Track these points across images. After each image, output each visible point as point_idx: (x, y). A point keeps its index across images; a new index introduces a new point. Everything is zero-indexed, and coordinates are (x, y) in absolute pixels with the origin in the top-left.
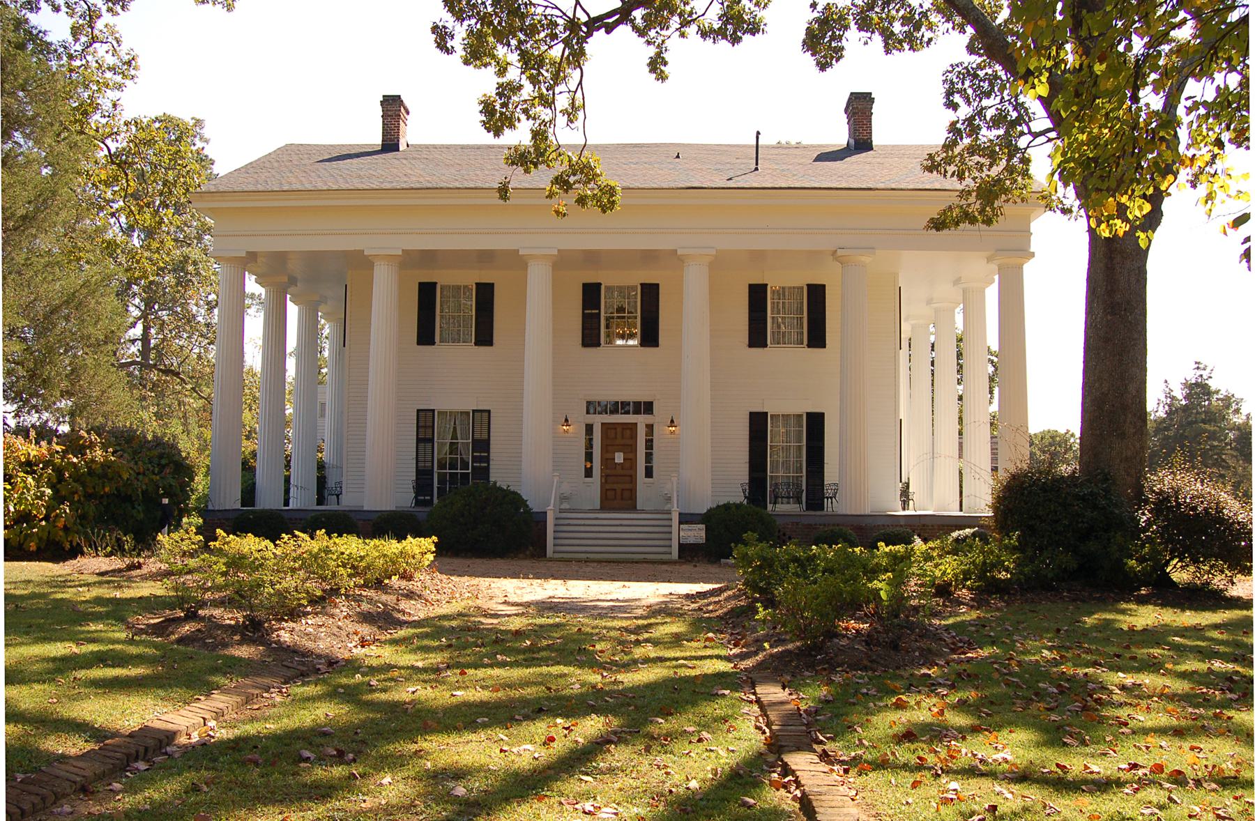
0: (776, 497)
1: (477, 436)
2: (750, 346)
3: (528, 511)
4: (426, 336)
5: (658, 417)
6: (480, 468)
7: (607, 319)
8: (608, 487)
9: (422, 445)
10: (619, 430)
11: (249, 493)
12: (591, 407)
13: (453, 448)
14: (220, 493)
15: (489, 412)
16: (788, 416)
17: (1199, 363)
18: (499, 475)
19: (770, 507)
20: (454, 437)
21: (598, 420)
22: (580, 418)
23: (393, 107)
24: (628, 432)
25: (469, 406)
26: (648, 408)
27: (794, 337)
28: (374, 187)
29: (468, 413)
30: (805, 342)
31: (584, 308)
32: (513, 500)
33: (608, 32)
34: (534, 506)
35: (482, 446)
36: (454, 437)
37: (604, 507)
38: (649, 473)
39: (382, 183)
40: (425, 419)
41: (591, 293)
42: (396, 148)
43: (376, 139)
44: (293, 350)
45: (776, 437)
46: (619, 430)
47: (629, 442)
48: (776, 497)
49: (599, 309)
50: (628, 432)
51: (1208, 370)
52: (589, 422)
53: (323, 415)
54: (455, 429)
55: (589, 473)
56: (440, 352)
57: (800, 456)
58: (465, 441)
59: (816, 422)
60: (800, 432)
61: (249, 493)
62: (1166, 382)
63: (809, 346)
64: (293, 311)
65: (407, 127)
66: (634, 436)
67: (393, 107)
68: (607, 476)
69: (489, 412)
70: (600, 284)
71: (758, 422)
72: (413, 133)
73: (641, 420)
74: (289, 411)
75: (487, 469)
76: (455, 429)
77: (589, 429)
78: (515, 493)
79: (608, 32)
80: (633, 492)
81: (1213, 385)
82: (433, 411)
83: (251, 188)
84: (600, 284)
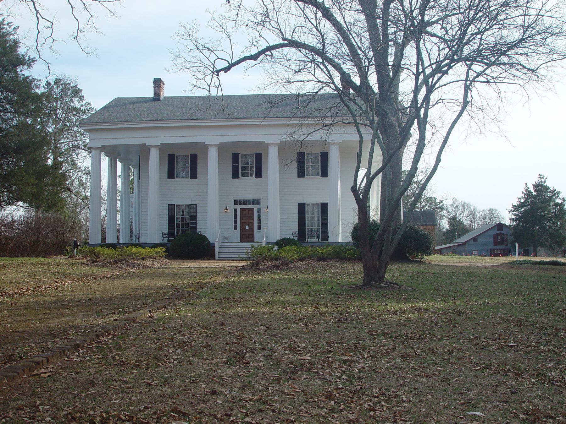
0: (309, 237)
1: (192, 214)
2: (298, 177)
3: (209, 242)
4: (171, 175)
5: (262, 206)
6: (193, 227)
7: (242, 167)
8: (243, 233)
9: (195, 214)
10: (247, 211)
11: (104, 238)
12: (236, 202)
13: (183, 219)
14: (357, 44)
15: (196, 205)
16: (314, 204)
17: (541, 175)
18: (200, 229)
19: (307, 240)
20: (183, 214)
21: (239, 207)
22: (232, 206)
23: (158, 83)
24: (251, 212)
25: (188, 202)
26: (258, 202)
27: (316, 173)
28: (149, 119)
29: (188, 205)
30: (320, 175)
31: (233, 163)
32: (204, 238)
33: (225, 72)
34: (211, 240)
35: (194, 218)
36: (183, 214)
37: (241, 241)
38: (259, 228)
39: (152, 117)
40: (171, 208)
41: (235, 157)
42: (159, 99)
43: (152, 95)
44: (120, 174)
45: (309, 215)
46: (247, 211)
47: (251, 215)
48: (309, 237)
49: (238, 163)
50: (251, 212)
51: (545, 178)
52: (235, 208)
53: (132, 207)
54: (183, 211)
55: (235, 228)
56: (176, 182)
57: (319, 220)
58: (187, 216)
59: (324, 207)
60: (319, 210)
61: (104, 238)
62: (526, 184)
63: (321, 177)
64: (119, 165)
65: (164, 86)
66: (253, 214)
67: (158, 83)
68: (243, 229)
69: (196, 205)
70: (239, 153)
71: (302, 207)
72: (167, 92)
73: (255, 207)
74: (119, 205)
75: (196, 227)
76: (183, 211)
77: (235, 210)
78: (204, 236)
79: (225, 72)
80: (253, 235)
81: (547, 184)
82: (174, 204)
83: (103, 121)
84: (239, 153)
